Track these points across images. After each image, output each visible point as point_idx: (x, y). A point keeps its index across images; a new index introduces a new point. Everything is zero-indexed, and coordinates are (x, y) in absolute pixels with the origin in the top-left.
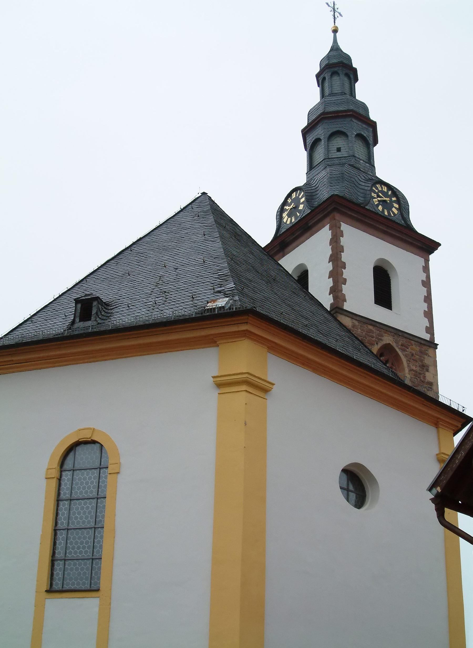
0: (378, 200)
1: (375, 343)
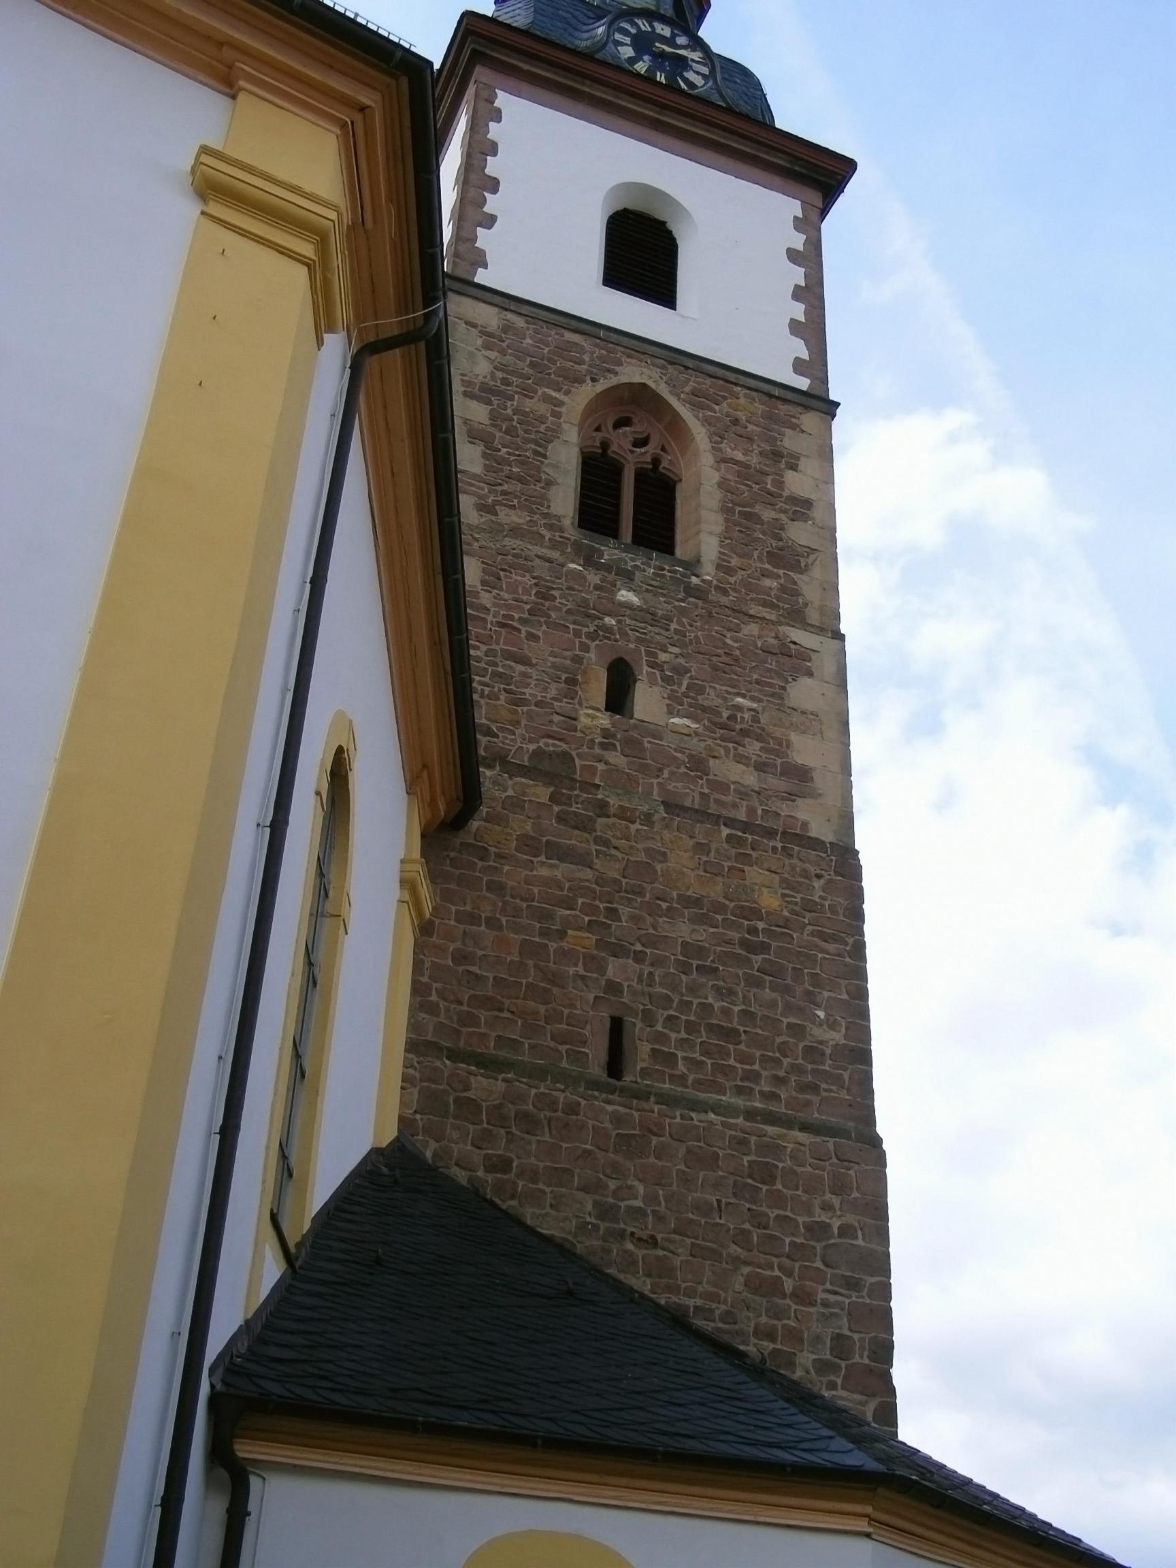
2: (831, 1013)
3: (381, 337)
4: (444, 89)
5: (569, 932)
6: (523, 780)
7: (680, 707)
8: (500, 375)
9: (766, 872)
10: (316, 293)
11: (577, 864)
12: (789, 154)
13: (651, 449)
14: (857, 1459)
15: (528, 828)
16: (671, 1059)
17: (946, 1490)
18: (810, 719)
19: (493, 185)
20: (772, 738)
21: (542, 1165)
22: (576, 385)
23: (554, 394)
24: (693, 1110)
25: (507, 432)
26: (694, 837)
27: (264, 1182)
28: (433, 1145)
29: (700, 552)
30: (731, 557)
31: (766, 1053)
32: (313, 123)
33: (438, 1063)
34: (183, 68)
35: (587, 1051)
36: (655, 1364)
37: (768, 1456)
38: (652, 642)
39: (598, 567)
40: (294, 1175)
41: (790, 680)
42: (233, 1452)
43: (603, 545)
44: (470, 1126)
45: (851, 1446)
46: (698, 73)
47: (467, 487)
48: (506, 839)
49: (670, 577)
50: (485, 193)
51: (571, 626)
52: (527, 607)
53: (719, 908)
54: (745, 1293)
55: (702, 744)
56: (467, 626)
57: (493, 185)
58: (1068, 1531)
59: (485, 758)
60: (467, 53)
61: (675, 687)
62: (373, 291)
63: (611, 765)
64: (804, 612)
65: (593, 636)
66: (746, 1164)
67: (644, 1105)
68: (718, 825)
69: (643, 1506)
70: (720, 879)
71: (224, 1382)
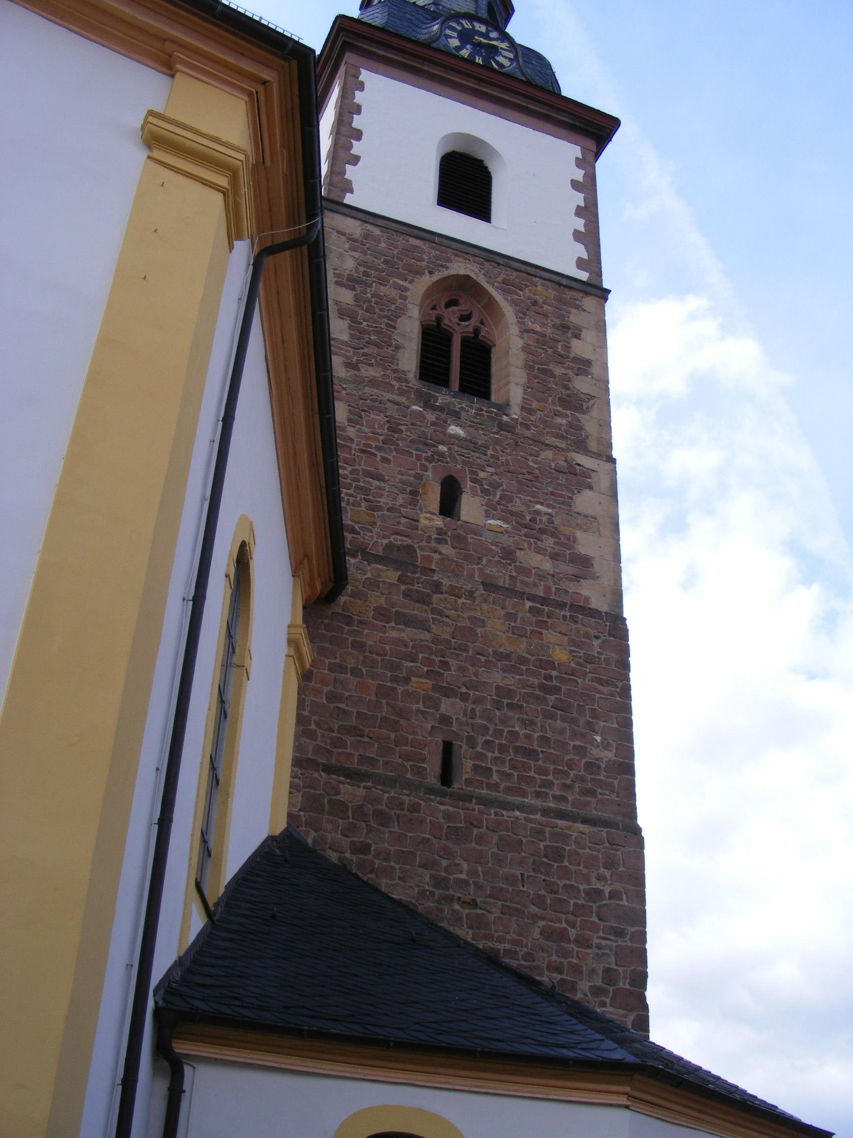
1: (426, 271)
2: (606, 738)
3: (275, 243)
4: (323, 69)
5: (413, 679)
6: (378, 566)
7: (495, 512)
8: (362, 269)
9: (558, 634)
10: (229, 211)
11: (418, 629)
12: (572, 114)
13: (473, 322)
14: (621, 1055)
15: (382, 601)
16: (488, 772)
17: (683, 1075)
18: (590, 521)
19: (358, 135)
20: (563, 535)
21: (392, 849)
22: (418, 276)
23: (401, 283)
24: (504, 809)
25: (367, 310)
26: (505, 609)
27: (190, 859)
28: (313, 834)
29: (509, 397)
30: (532, 402)
31: (557, 767)
32: (228, 93)
33: (316, 775)
34: (141, 58)
35: (426, 766)
36: (475, 990)
37: (557, 1054)
38: (473, 464)
39: (434, 408)
40: (212, 854)
41: (576, 492)
42: (171, 1049)
43: (437, 393)
44: (340, 820)
45: (616, 1046)
46: (505, 57)
47: (337, 350)
48: (366, 610)
49: (487, 416)
50: (352, 141)
51: (414, 452)
52: (382, 438)
53: (523, 661)
54: (541, 940)
55: (511, 540)
56: (337, 452)
57: (358, 135)
58: (769, 1101)
59: (349, 550)
60: (339, 43)
61: (491, 497)
62: (271, 210)
63: (443, 555)
64: (586, 442)
65: (430, 460)
66: (542, 848)
67: (468, 805)
68: (524, 600)
69: (466, 1088)
70: (524, 639)
71: (164, 999)
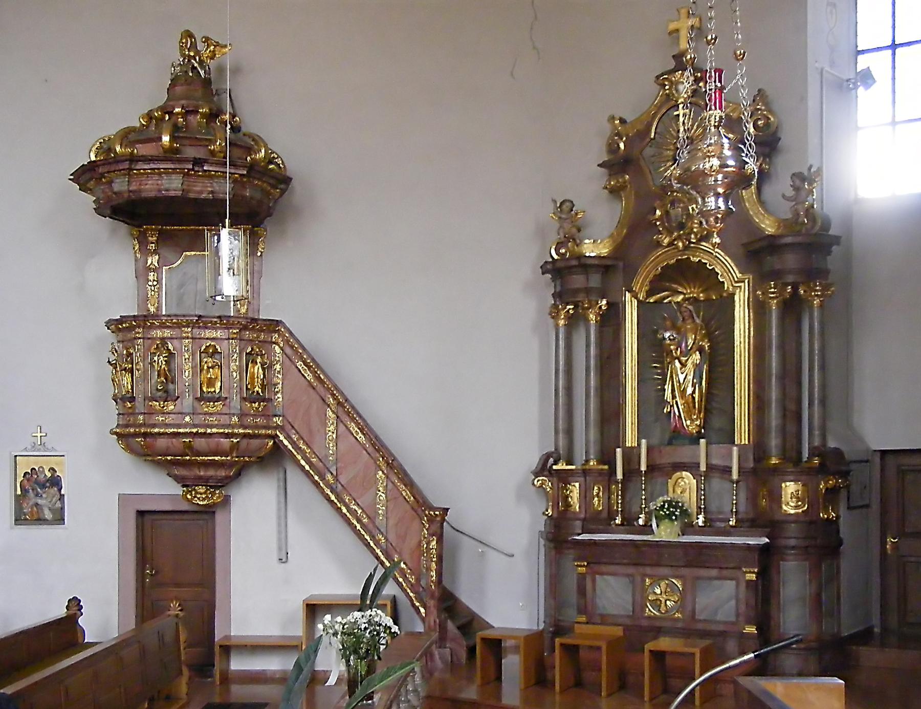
0: (200, 471)
